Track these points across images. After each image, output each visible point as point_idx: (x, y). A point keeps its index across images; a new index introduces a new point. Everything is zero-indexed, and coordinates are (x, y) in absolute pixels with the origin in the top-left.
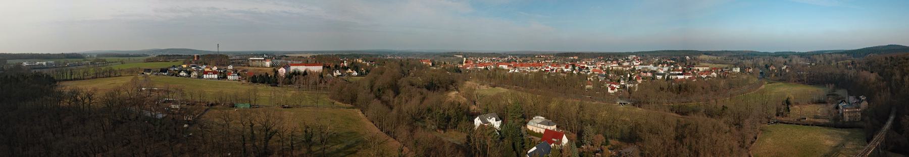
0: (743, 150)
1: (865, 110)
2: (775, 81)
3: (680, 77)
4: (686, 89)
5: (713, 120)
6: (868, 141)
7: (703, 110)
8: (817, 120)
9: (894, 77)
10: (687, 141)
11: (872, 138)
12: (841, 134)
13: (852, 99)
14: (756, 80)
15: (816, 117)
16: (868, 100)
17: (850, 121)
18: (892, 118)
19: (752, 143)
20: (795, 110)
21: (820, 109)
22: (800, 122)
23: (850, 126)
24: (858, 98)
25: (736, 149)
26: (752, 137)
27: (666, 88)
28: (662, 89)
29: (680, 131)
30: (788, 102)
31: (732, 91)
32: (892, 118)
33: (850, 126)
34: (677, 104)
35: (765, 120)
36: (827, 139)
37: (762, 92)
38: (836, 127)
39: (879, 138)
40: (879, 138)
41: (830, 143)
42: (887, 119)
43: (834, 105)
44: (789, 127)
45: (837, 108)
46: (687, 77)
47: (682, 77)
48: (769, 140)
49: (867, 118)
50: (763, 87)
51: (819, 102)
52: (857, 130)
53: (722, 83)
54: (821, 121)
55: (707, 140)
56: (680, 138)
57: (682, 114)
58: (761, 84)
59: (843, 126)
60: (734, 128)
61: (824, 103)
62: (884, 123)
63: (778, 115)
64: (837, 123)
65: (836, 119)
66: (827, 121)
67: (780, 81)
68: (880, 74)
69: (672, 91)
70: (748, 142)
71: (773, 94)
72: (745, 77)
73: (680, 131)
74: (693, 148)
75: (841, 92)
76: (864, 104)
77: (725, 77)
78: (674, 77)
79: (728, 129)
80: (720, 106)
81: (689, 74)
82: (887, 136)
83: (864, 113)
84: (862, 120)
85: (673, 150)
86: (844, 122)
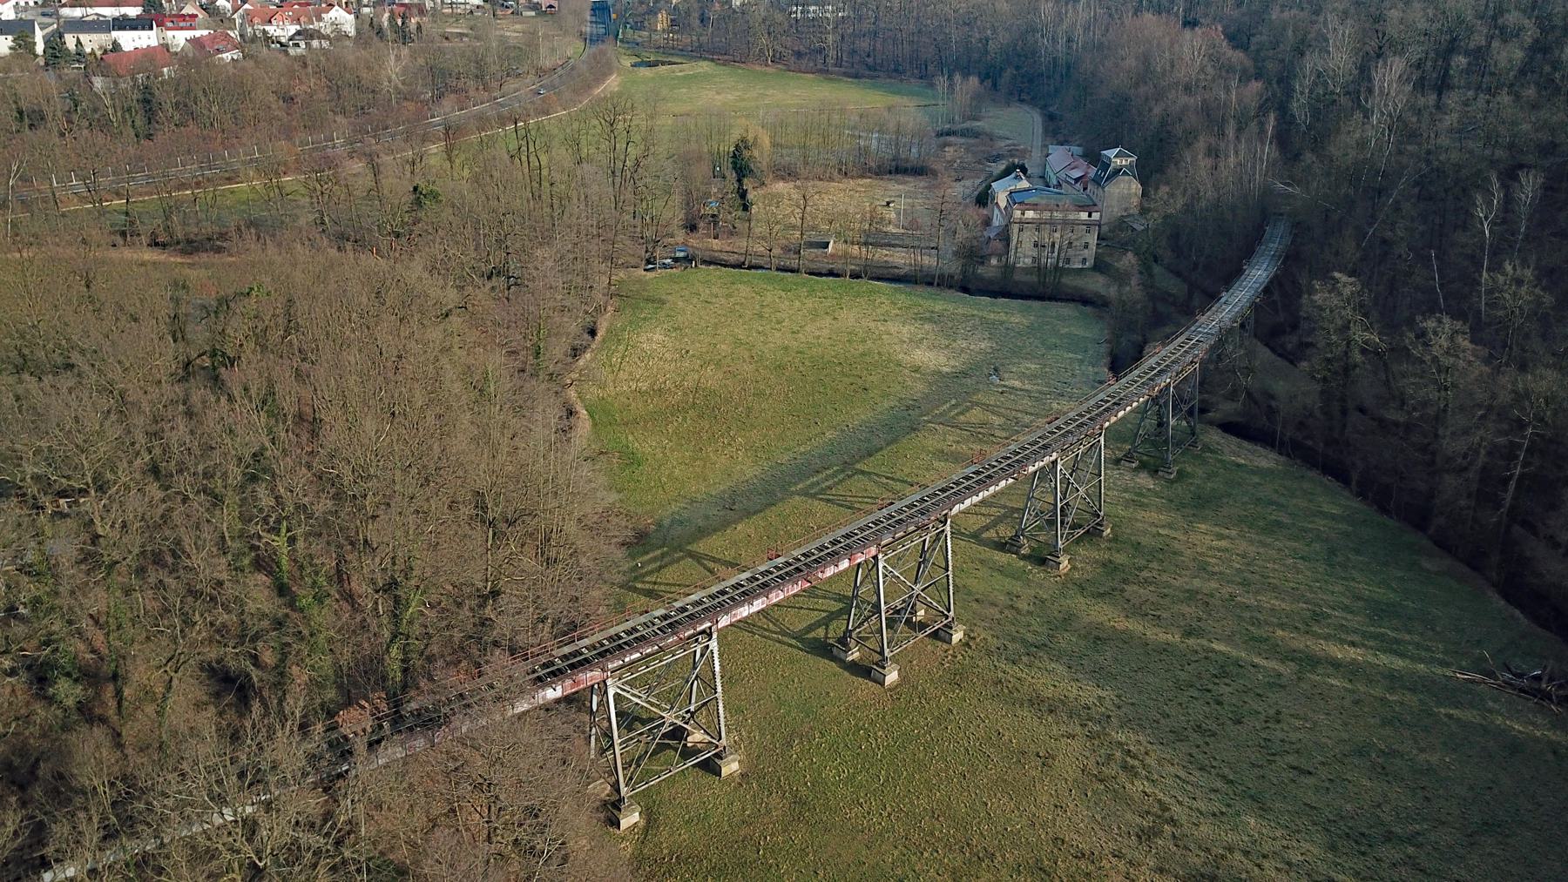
0: (540, 387)
1: (1121, 224)
2: (667, 54)
3: (130, 40)
4: (187, 110)
5: (369, 261)
6: (1118, 366)
7: (306, 219)
8: (881, 255)
9: (1311, 62)
10: (247, 374)
11: (1138, 356)
12: (990, 327)
13: (1061, 159)
14: (573, 48)
15: (874, 239)
16: (1147, 173)
17: (1039, 269)
18: (1258, 274)
19: (576, 352)
20: (778, 204)
21: (897, 202)
22: (806, 263)
23: (1043, 288)
24: (1093, 157)
25: (502, 384)
26: (573, 326)
27: (59, 106)
28: (31, 118)
29: (199, 335)
30: (740, 166)
31: (449, 110)
32: (1258, 274)
33: (1043, 288)
34: (147, 201)
35: (630, 249)
36: (916, 342)
37: (612, 114)
38: (967, 286)
39: (1173, 359)
40: (1173, 359)
41: (930, 358)
42: (1231, 275)
43: (970, 185)
44: (745, 287)
45: (984, 198)
46: (179, 38)
47: (145, 39)
48: (654, 339)
49: (1128, 260)
50: (613, 83)
51: (899, 169)
52: (1066, 310)
53: (394, 65)
54: (900, 259)
55: (352, 357)
56: (209, 369)
57: (191, 247)
58: (601, 70)
59: (1005, 289)
60: (482, 294)
61: (918, 171)
62: (1212, 297)
63: (692, 228)
64: (978, 276)
65: (972, 254)
66: (929, 261)
67: (698, 52)
68: (1237, 38)
69: (104, 125)
70: (557, 349)
71: (665, 121)
72: (512, 31)
73: (199, 335)
74: (289, 406)
75: (1016, 124)
76: (1127, 189)
77: (403, 36)
78: (92, 42)
79: (452, 297)
80: (396, 185)
81: (188, 21)
82: (1217, 351)
83: (1113, 237)
84: (1100, 266)
85: (179, 433)
86: (1008, 269)
